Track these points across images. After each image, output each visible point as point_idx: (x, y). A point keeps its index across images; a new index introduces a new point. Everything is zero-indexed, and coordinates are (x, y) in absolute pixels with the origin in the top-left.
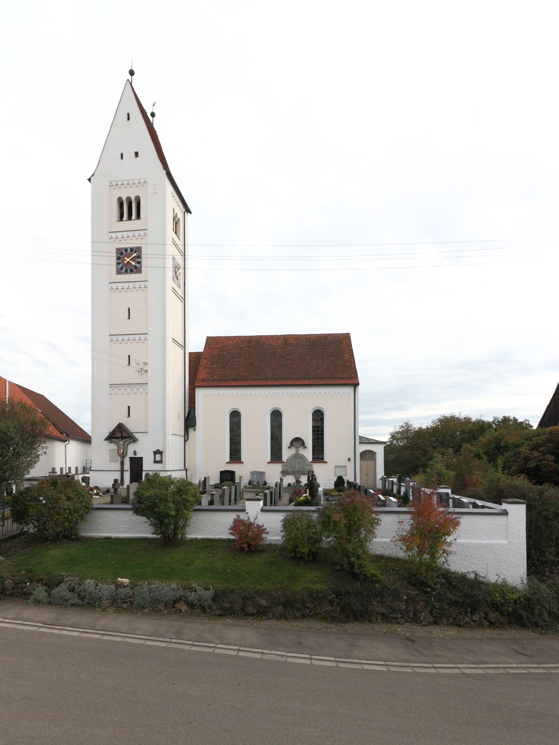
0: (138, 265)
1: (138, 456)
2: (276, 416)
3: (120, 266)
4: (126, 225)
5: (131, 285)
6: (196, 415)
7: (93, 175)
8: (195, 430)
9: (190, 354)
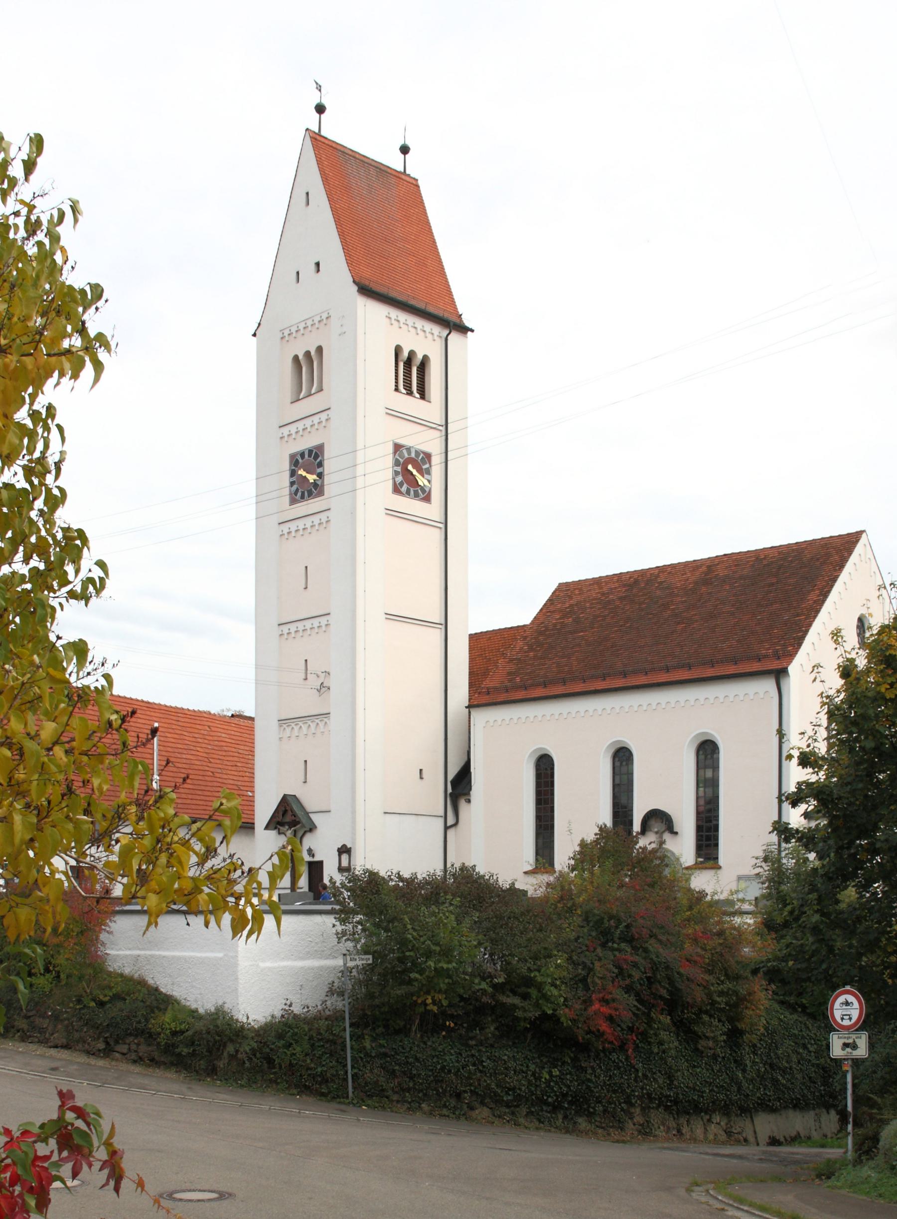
1: (316, 859)
3: (295, 487)
5: (308, 522)
6: (472, 770)
7: (259, 324)
8: (469, 801)
9: (477, 641)
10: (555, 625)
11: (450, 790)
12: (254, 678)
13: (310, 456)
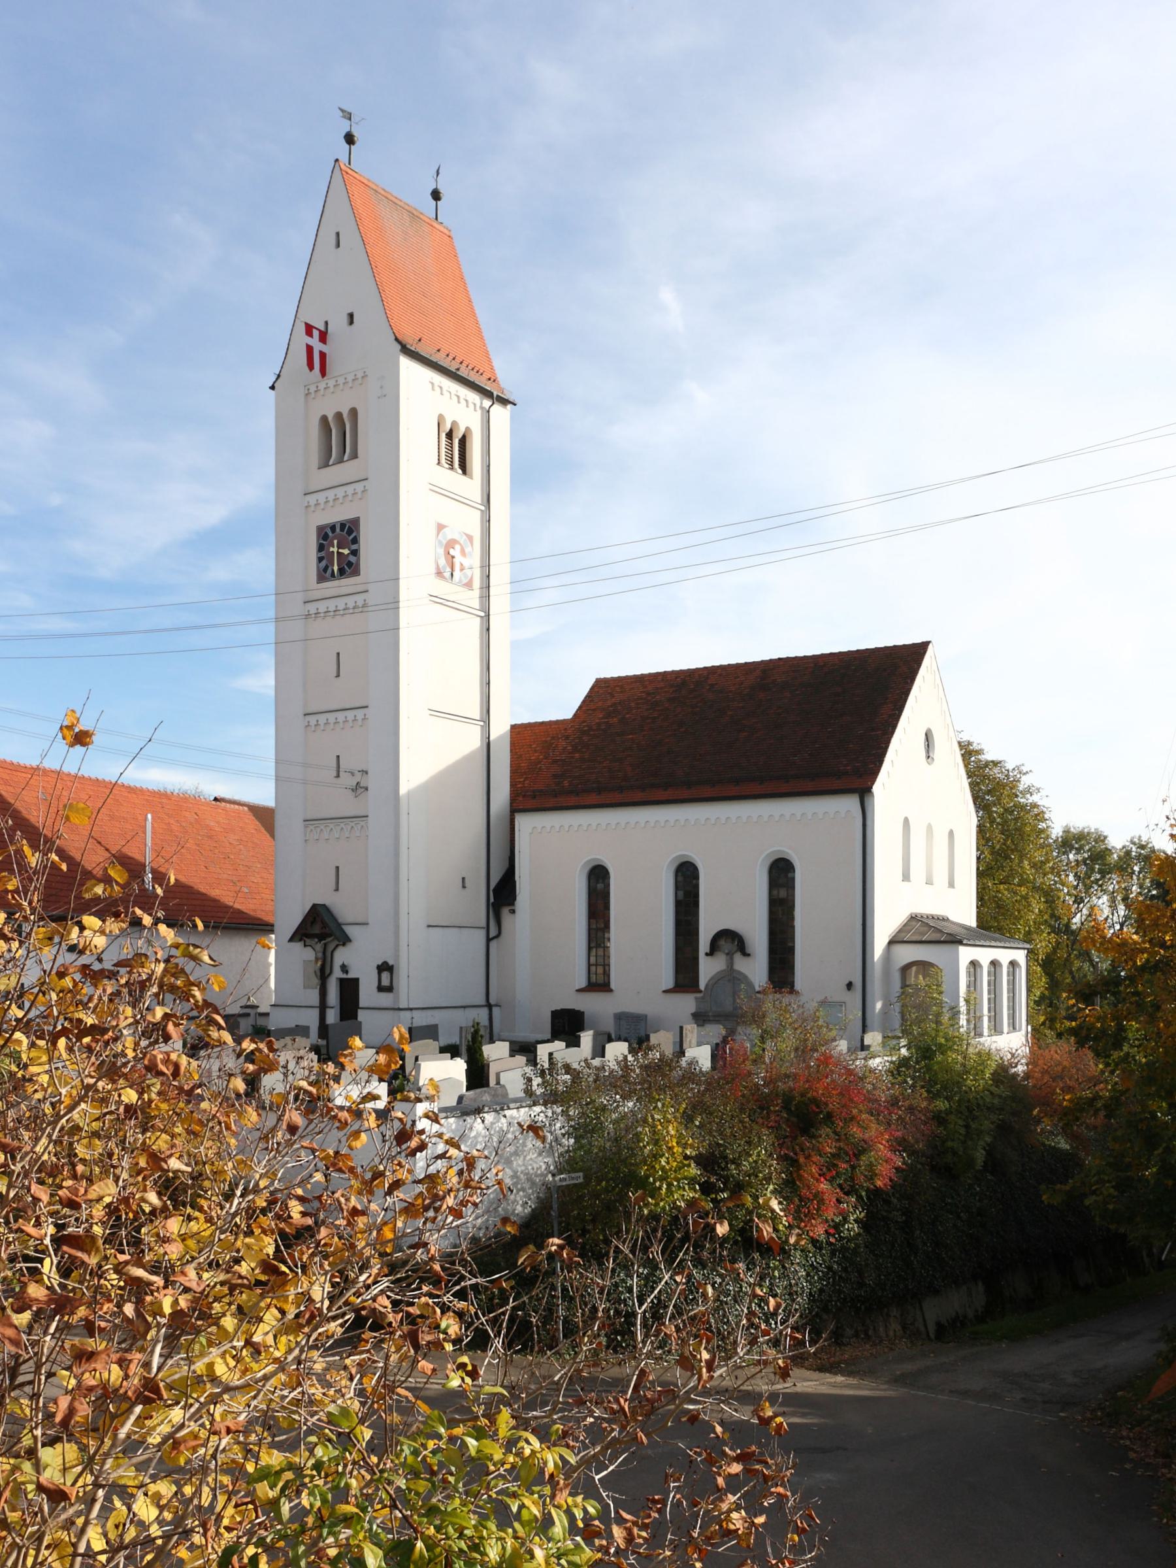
0: (352, 559)
2: (687, 877)
3: (324, 563)
4: (337, 473)
7: (279, 376)
8: (513, 912)
10: (599, 724)
11: (492, 900)
12: (273, 773)
13: (342, 529)
